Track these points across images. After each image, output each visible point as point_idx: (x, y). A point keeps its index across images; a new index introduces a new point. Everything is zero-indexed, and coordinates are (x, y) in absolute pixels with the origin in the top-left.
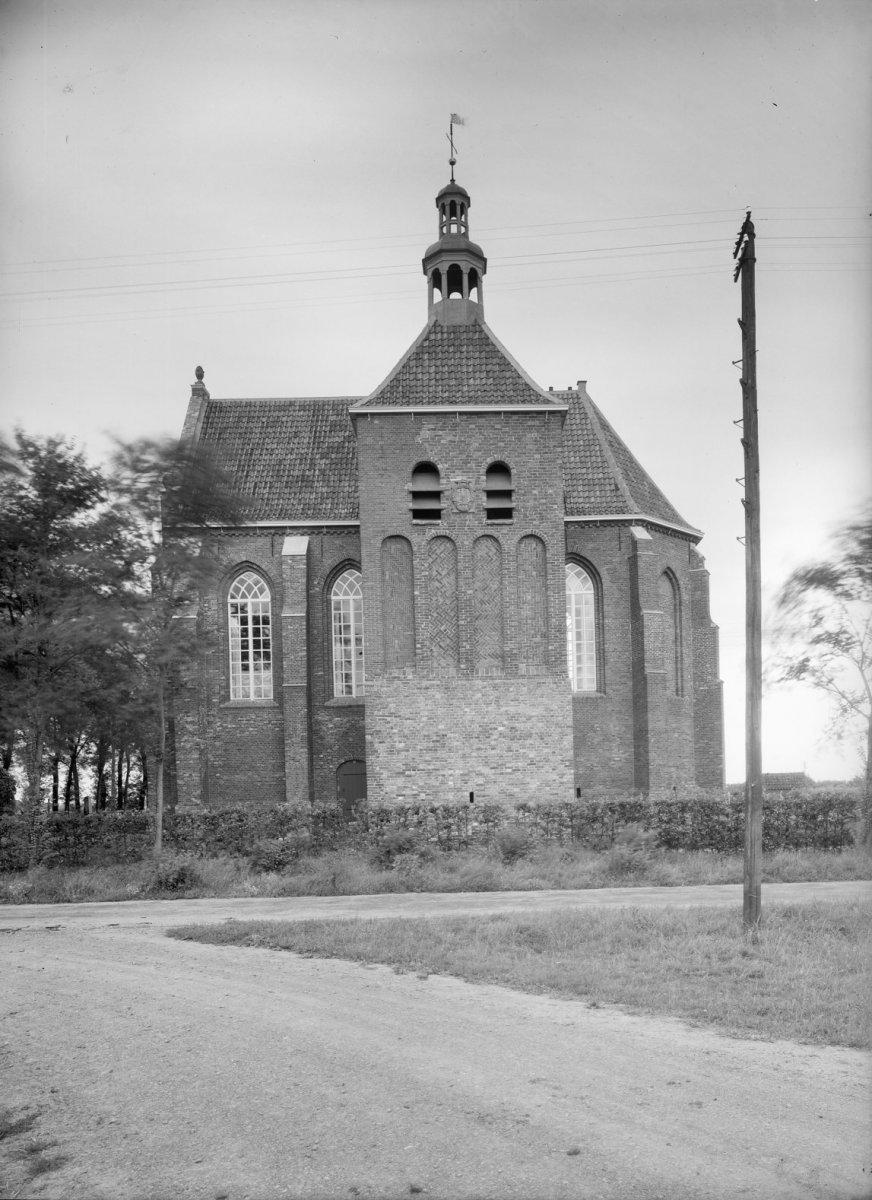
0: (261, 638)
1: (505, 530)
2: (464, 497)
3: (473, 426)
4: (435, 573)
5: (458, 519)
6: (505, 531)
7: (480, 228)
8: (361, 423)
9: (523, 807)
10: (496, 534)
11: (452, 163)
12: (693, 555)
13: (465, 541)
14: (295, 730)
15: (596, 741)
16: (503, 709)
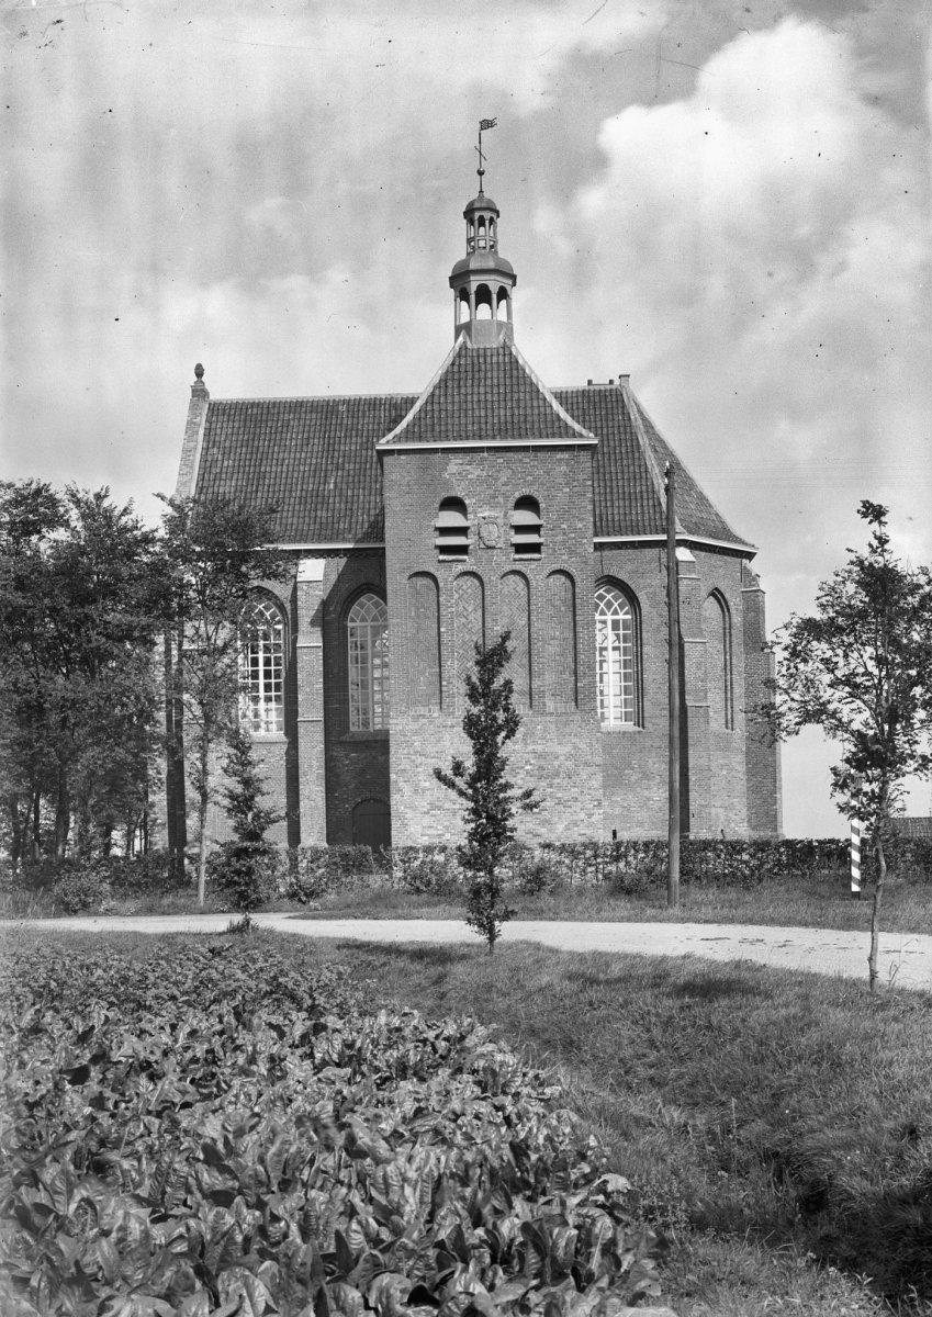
0: (273, 668)
1: (533, 565)
2: (493, 534)
3: (502, 460)
4: (461, 608)
5: (485, 555)
6: (533, 567)
7: (510, 242)
8: (386, 460)
9: (547, 846)
10: (523, 570)
11: (481, 173)
12: (745, 572)
13: (491, 578)
14: (311, 766)
15: (633, 779)
16: (530, 748)
